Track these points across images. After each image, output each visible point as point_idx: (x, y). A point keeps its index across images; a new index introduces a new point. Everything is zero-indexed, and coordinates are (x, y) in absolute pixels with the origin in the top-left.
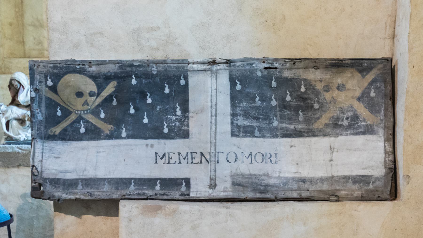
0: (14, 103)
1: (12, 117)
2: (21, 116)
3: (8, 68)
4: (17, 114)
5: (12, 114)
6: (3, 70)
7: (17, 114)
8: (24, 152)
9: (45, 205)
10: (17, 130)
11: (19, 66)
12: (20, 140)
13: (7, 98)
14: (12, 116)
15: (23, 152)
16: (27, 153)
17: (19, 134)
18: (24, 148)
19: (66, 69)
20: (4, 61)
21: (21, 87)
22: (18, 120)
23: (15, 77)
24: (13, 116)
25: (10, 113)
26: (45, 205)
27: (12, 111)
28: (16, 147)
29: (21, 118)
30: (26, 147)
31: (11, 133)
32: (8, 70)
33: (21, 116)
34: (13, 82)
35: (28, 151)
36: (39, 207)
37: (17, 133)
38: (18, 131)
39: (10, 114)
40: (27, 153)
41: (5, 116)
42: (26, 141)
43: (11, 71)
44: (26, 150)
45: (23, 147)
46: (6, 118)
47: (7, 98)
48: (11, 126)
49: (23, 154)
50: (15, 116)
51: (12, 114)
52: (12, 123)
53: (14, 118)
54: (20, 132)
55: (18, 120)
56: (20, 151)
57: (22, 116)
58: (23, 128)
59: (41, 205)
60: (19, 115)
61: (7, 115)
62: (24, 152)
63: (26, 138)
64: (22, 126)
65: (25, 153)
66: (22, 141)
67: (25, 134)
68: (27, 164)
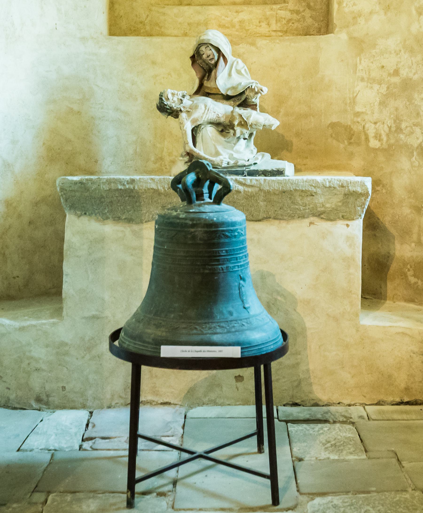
0: (202, 90)
1: (206, 120)
2: (223, 117)
3: (157, 24)
4: (216, 113)
5: (207, 114)
6: (148, 28)
7: (216, 113)
8: (250, 190)
9: (283, 300)
10: (215, 146)
11: (180, 20)
12: (221, 166)
13: (161, 83)
14: (208, 117)
15: (247, 189)
16: (254, 193)
17: (217, 154)
18: (248, 182)
19: (237, 31)
20: (150, 10)
21: (221, 58)
22: (217, 124)
23: (209, 40)
24: (208, 115)
25: (203, 111)
26: (283, 300)
27: (206, 106)
28: (232, 179)
29: (222, 120)
30: (253, 179)
31: (200, 150)
32: (157, 28)
33: (224, 117)
34: (203, 48)
35: (257, 187)
36: (272, 306)
37: (213, 151)
38: (216, 148)
39: (203, 114)
40: (254, 193)
41: (192, 117)
42: (232, 167)
43: (163, 30)
44: (252, 186)
45: (247, 179)
46: (193, 121)
47: (161, 83)
48: (202, 136)
49: (247, 195)
50: (212, 116)
51: (207, 114)
52: (203, 132)
53: (209, 121)
54: (220, 149)
55: (217, 124)
56: (241, 188)
57: (226, 118)
58: (225, 141)
59: (276, 300)
60: (220, 115)
61: (196, 115)
62: (250, 190)
63: (232, 162)
64: (224, 136)
65: (252, 192)
66: (225, 168)
67: (228, 153)
68: (253, 216)
